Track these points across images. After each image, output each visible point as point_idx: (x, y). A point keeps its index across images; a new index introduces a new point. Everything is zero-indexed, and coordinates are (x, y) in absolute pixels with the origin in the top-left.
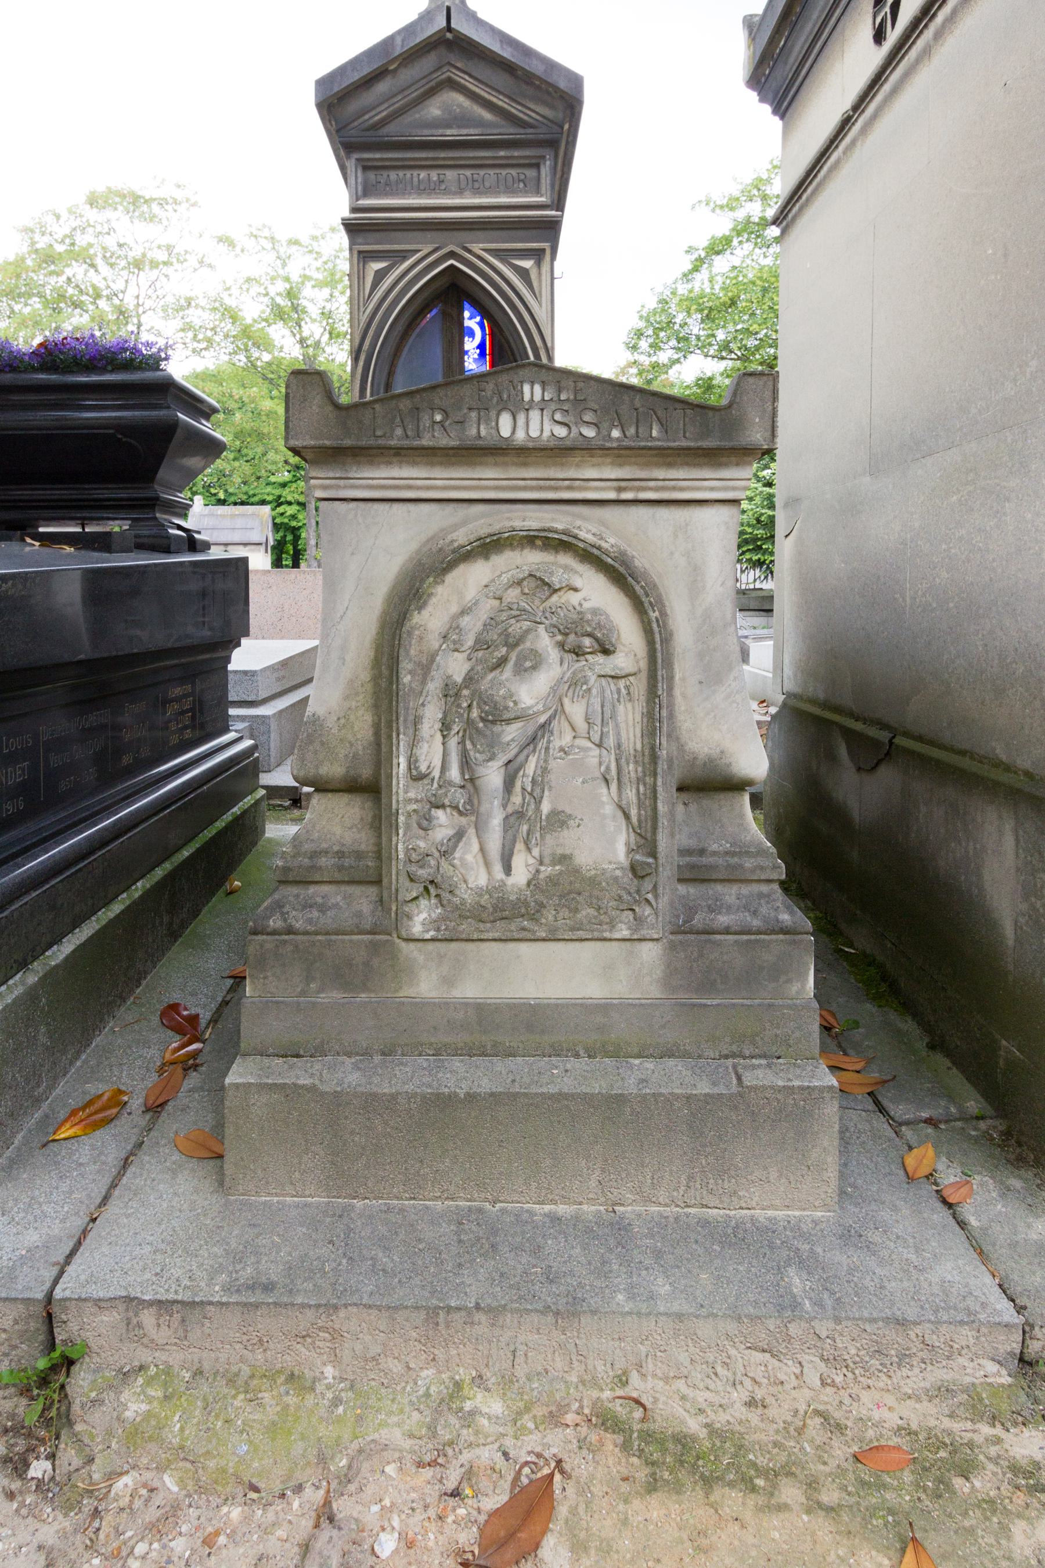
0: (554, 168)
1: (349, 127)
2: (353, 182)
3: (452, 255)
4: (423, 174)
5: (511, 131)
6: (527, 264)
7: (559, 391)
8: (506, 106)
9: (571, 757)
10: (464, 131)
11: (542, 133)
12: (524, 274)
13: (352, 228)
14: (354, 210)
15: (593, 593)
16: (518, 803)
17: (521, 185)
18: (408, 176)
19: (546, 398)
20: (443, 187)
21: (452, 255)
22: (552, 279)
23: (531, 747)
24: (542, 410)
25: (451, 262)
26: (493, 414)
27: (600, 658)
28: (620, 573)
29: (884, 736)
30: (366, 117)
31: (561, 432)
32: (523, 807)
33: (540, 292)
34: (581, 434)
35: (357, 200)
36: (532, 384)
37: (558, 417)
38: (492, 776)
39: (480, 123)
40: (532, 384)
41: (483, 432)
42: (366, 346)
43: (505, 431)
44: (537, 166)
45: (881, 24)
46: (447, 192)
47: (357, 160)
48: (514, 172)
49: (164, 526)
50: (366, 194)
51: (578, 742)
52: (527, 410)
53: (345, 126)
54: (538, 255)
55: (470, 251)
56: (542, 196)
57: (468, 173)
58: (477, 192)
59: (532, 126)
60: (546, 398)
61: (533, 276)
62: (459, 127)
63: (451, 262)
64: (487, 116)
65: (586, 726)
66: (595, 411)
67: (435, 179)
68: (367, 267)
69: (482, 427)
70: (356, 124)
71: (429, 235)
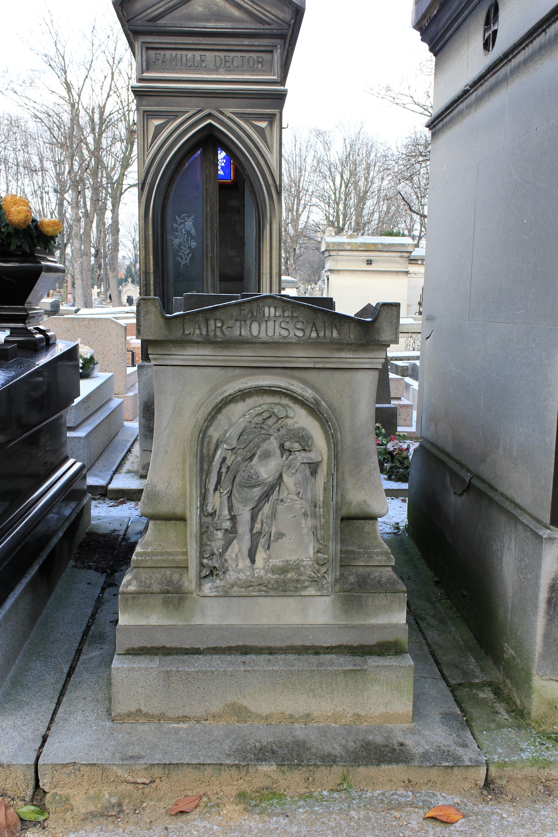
0: (282, 55)
1: (136, 19)
2: (140, 59)
3: (210, 116)
4: (190, 54)
5: (253, 26)
6: (263, 124)
7: (284, 311)
8: (249, 7)
9: (286, 504)
10: (220, 25)
11: (274, 28)
12: (261, 131)
13: (138, 93)
14: (140, 80)
15: (301, 419)
16: (259, 527)
17: (260, 66)
18: (179, 56)
19: (277, 315)
20: (204, 65)
21: (210, 116)
22: (281, 128)
23: (266, 499)
24: (275, 321)
25: (209, 121)
26: (248, 322)
27: (303, 454)
28: (313, 409)
29: (468, 477)
30: (149, 11)
31: (285, 333)
32: (262, 529)
33: (272, 145)
34: (295, 335)
35: (142, 73)
36: (269, 307)
37: (283, 325)
38: (245, 515)
39: (232, 19)
40: (269, 307)
41: (243, 333)
42: (149, 181)
43: (255, 333)
44: (271, 52)
45: (487, 39)
46: (208, 70)
47: (142, 42)
48: (254, 55)
49: (32, 334)
50: (148, 70)
51: (290, 496)
52: (267, 321)
53: (132, 19)
54: (271, 118)
55: (222, 113)
56: (273, 75)
57: (222, 54)
58: (229, 70)
59: (268, 24)
60: (277, 315)
61: (267, 132)
62: (217, 21)
63: (209, 121)
64: (236, 13)
65: (295, 488)
66: (303, 322)
67: (198, 59)
68: (150, 122)
69: (242, 330)
70: (141, 16)
71: (194, 100)
